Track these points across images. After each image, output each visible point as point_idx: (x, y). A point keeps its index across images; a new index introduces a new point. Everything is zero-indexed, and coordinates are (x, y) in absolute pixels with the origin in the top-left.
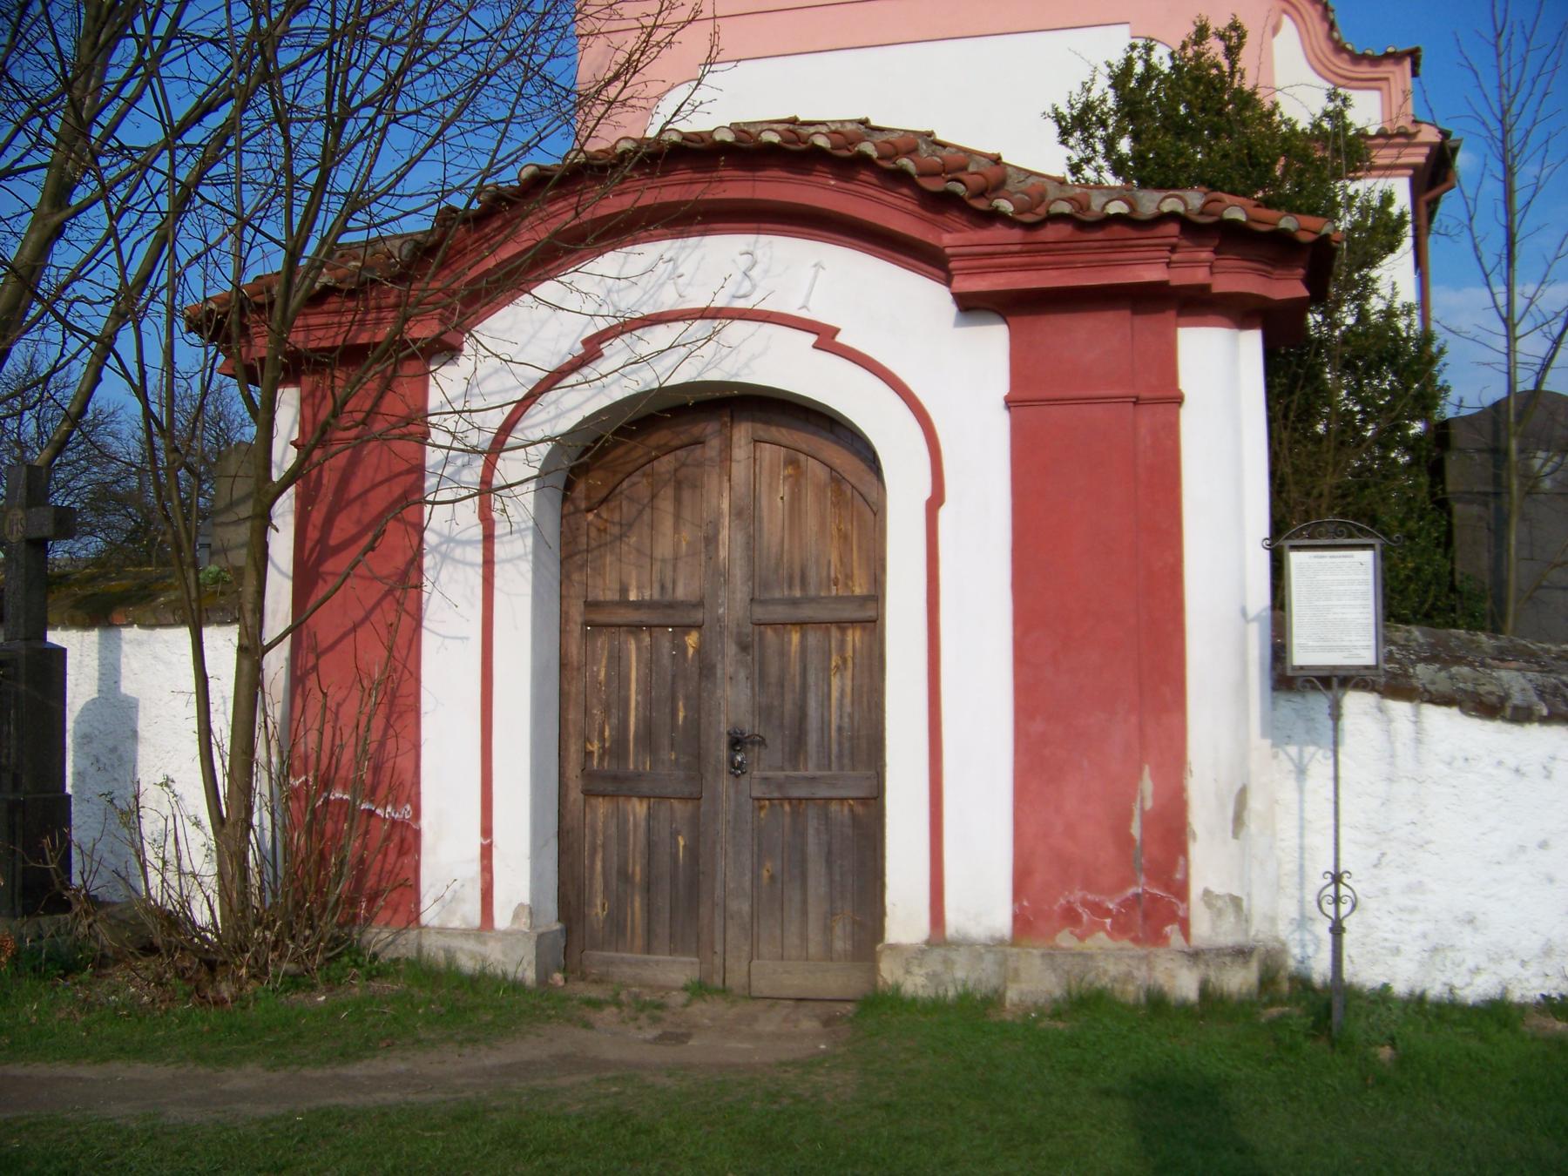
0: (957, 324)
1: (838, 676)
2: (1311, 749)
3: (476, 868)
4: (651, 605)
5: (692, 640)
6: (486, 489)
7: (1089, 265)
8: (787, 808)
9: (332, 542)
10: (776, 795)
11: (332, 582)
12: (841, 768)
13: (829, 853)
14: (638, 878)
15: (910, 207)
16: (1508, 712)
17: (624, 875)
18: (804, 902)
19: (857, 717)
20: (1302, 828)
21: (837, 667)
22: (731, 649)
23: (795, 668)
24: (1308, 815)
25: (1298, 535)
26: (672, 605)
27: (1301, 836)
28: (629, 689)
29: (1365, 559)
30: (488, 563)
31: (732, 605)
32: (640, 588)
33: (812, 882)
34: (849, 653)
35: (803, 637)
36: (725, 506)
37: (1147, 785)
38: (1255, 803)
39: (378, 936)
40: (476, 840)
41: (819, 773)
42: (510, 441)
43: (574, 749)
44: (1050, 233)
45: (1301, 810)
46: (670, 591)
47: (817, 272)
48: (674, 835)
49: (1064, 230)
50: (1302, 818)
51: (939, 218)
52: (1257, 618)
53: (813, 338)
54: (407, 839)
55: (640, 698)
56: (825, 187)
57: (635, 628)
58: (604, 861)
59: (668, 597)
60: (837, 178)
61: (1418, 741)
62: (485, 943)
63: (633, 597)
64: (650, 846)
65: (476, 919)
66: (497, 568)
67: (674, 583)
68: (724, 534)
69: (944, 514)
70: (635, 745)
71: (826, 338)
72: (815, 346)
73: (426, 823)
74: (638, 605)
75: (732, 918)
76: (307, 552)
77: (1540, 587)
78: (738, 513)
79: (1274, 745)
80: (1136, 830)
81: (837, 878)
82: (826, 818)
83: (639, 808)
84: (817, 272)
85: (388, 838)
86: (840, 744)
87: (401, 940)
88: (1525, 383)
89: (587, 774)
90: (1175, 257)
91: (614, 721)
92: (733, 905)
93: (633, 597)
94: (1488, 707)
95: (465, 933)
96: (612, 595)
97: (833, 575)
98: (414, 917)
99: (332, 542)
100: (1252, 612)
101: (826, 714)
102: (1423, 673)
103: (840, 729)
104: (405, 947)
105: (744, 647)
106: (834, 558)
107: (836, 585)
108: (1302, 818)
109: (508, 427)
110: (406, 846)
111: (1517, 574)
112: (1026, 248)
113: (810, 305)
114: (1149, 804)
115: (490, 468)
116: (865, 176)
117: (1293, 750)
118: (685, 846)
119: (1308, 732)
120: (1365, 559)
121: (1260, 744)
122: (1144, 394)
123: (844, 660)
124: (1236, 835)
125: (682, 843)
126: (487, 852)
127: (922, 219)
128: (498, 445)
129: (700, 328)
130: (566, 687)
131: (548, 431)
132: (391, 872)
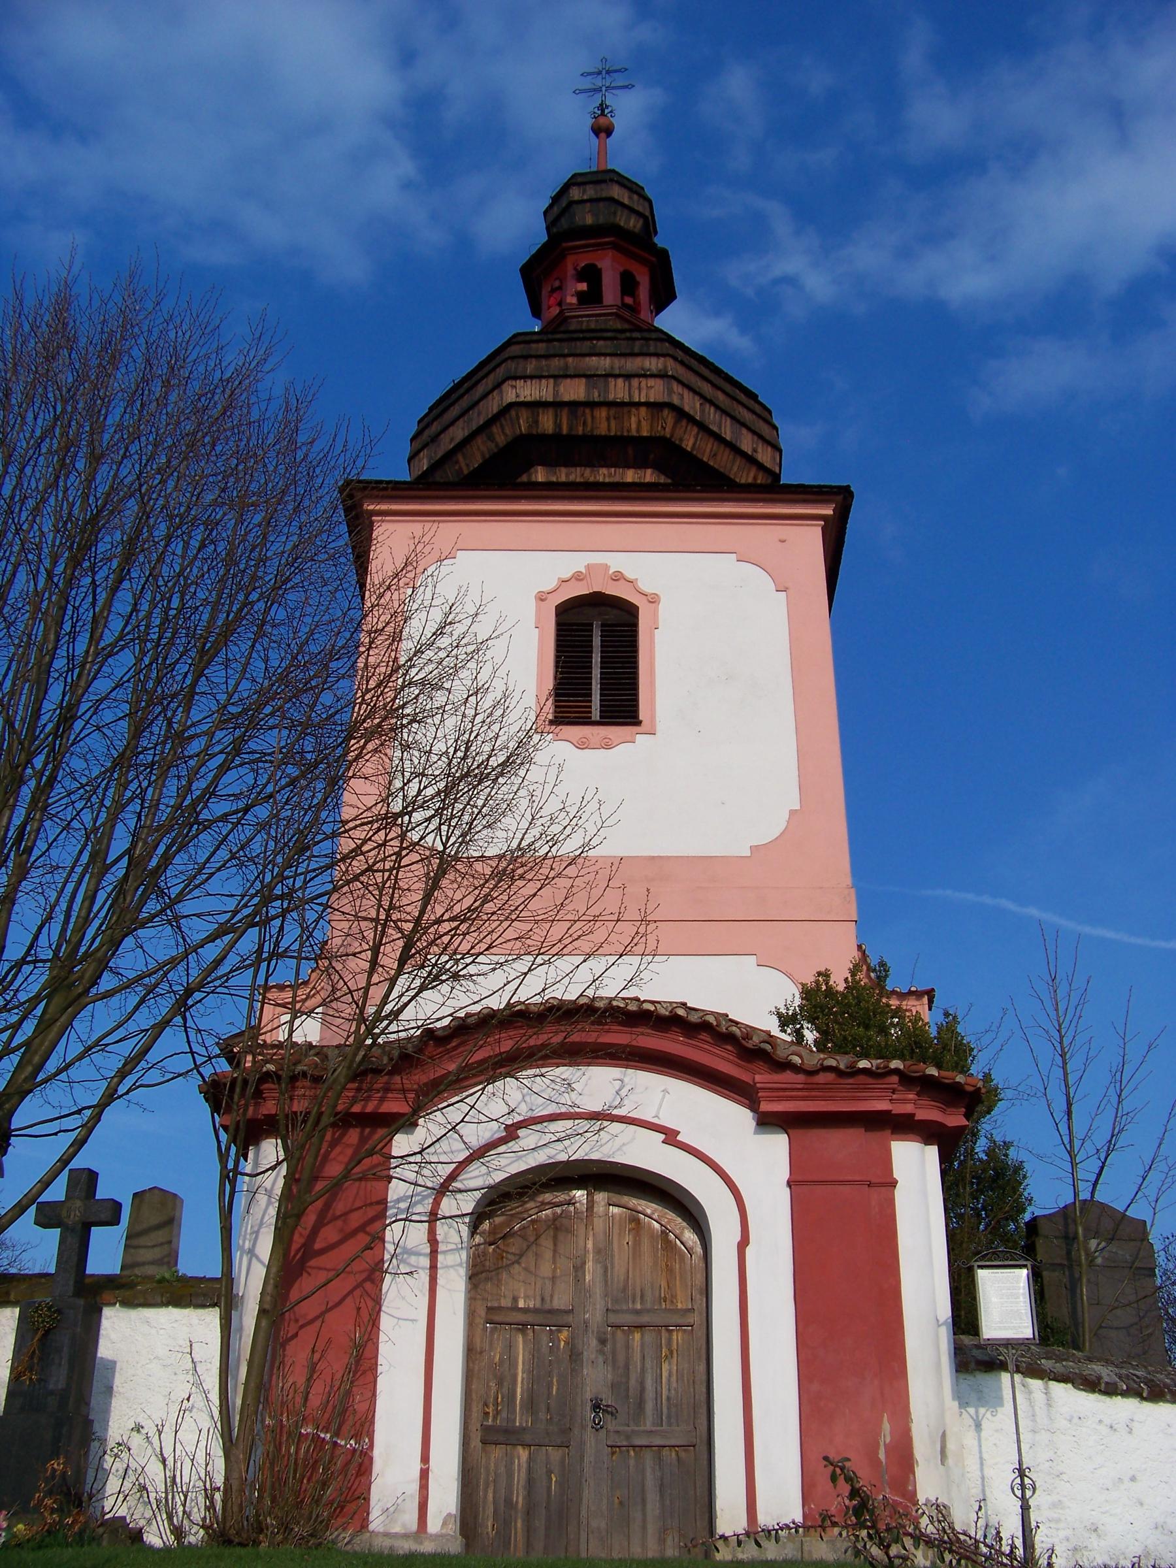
0: (756, 1133)
1: (667, 1362)
2: (982, 1410)
3: (416, 1486)
4: (536, 1311)
5: (564, 1335)
6: (433, 1217)
7: (843, 1099)
8: (632, 1453)
9: (317, 1246)
10: (625, 1443)
11: (323, 1277)
12: (670, 1424)
13: (662, 1485)
14: (520, 1505)
15: (731, 1057)
16: (1103, 1387)
17: (509, 1503)
18: (644, 1521)
19: (680, 1390)
20: (982, 1464)
21: (666, 1356)
22: (594, 1343)
23: (637, 1357)
24: (985, 1456)
25: (983, 1258)
26: (551, 1312)
27: (982, 1470)
28: (516, 1368)
29: (1024, 1272)
30: (433, 1268)
31: (594, 1314)
32: (526, 1297)
33: (649, 1507)
34: (675, 1346)
35: (642, 1336)
36: (590, 1245)
37: (886, 1426)
38: (951, 1446)
39: (344, 1537)
40: (417, 1466)
41: (654, 1429)
42: (456, 1185)
43: (476, 1409)
44: (822, 1078)
45: (980, 1452)
46: (548, 1301)
47: (664, 1096)
48: (549, 1472)
49: (830, 1077)
50: (981, 1458)
51: (749, 1065)
52: (945, 1323)
53: (663, 1137)
54: (362, 1465)
55: (525, 1375)
56: (678, 1041)
57: (523, 1327)
58: (494, 1492)
59: (547, 1306)
60: (685, 1036)
61: (1049, 1405)
62: (421, 1543)
63: (521, 1304)
64: (530, 1482)
65: (413, 1526)
66: (440, 1272)
67: (552, 1296)
68: (589, 1265)
69: (749, 1251)
70: (520, 1409)
71: (670, 1137)
72: (678, 1133)
73: (377, 1453)
74: (525, 1310)
75: (593, 1532)
76: (292, 1254)
77: (1101, 1327)
78: (598, 1251)
79: (960, 1407)
80: (882, 1455)
81: (668, 1502)
82: (659, 1459)
83: (523, 1454)
84: (664, 1096)
85: (347, 1464)
86: (669, 1408)
87: (357, 1540)
88: (1084, 1195)
89: (486, 1429)
90: (894, 1096)
91: (505, 1390)
92: (594, 1524)
93: (521, 1304)
94: (1091, 1385)
95: (406, 1536)
96: (506, 1302)
97: (663, 1295)
98: (364, 1524)
99: (317, 1246)
100: (942, 1320)
101: (659, 1388)
102: (1046, 1364)
103: (668, 1399)
104: (360, 1544)
105: (603, 1342)
106: (664, 1284)
107: (665, 1301)
108: (981, 1458)
109: (452, 1177)
110: (363, 1469)
111: (1088, 1317)
112: (806, 1086)
113: (660, 1116)
114: (888, 1440)
115: (437, 1204)
116: (704, 1036)
117: (972, 1410)
118: (556, 1482)
119: (979, 1399)
120: (1024, 1272)
121: (952, 1405)
122: (874, 1180)
123: (671, 1352)
124: (943, 1463)
125: (554, 1479)
126: (424, 1474)
127: (738, 1065)
128: (443, 1189)
129: (584, 1125)
130: (471, 1365)
131: (478, 1183)
132: (350, 1489)
